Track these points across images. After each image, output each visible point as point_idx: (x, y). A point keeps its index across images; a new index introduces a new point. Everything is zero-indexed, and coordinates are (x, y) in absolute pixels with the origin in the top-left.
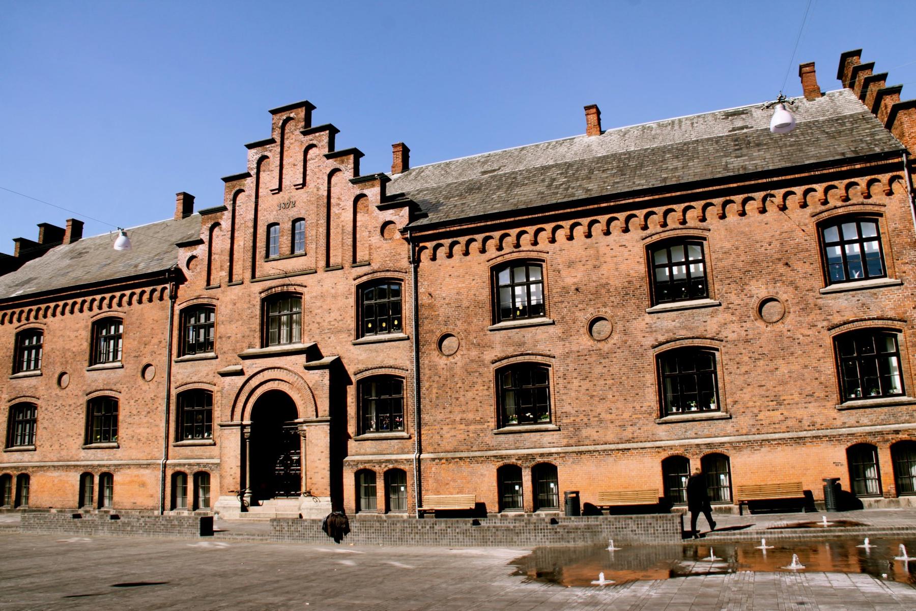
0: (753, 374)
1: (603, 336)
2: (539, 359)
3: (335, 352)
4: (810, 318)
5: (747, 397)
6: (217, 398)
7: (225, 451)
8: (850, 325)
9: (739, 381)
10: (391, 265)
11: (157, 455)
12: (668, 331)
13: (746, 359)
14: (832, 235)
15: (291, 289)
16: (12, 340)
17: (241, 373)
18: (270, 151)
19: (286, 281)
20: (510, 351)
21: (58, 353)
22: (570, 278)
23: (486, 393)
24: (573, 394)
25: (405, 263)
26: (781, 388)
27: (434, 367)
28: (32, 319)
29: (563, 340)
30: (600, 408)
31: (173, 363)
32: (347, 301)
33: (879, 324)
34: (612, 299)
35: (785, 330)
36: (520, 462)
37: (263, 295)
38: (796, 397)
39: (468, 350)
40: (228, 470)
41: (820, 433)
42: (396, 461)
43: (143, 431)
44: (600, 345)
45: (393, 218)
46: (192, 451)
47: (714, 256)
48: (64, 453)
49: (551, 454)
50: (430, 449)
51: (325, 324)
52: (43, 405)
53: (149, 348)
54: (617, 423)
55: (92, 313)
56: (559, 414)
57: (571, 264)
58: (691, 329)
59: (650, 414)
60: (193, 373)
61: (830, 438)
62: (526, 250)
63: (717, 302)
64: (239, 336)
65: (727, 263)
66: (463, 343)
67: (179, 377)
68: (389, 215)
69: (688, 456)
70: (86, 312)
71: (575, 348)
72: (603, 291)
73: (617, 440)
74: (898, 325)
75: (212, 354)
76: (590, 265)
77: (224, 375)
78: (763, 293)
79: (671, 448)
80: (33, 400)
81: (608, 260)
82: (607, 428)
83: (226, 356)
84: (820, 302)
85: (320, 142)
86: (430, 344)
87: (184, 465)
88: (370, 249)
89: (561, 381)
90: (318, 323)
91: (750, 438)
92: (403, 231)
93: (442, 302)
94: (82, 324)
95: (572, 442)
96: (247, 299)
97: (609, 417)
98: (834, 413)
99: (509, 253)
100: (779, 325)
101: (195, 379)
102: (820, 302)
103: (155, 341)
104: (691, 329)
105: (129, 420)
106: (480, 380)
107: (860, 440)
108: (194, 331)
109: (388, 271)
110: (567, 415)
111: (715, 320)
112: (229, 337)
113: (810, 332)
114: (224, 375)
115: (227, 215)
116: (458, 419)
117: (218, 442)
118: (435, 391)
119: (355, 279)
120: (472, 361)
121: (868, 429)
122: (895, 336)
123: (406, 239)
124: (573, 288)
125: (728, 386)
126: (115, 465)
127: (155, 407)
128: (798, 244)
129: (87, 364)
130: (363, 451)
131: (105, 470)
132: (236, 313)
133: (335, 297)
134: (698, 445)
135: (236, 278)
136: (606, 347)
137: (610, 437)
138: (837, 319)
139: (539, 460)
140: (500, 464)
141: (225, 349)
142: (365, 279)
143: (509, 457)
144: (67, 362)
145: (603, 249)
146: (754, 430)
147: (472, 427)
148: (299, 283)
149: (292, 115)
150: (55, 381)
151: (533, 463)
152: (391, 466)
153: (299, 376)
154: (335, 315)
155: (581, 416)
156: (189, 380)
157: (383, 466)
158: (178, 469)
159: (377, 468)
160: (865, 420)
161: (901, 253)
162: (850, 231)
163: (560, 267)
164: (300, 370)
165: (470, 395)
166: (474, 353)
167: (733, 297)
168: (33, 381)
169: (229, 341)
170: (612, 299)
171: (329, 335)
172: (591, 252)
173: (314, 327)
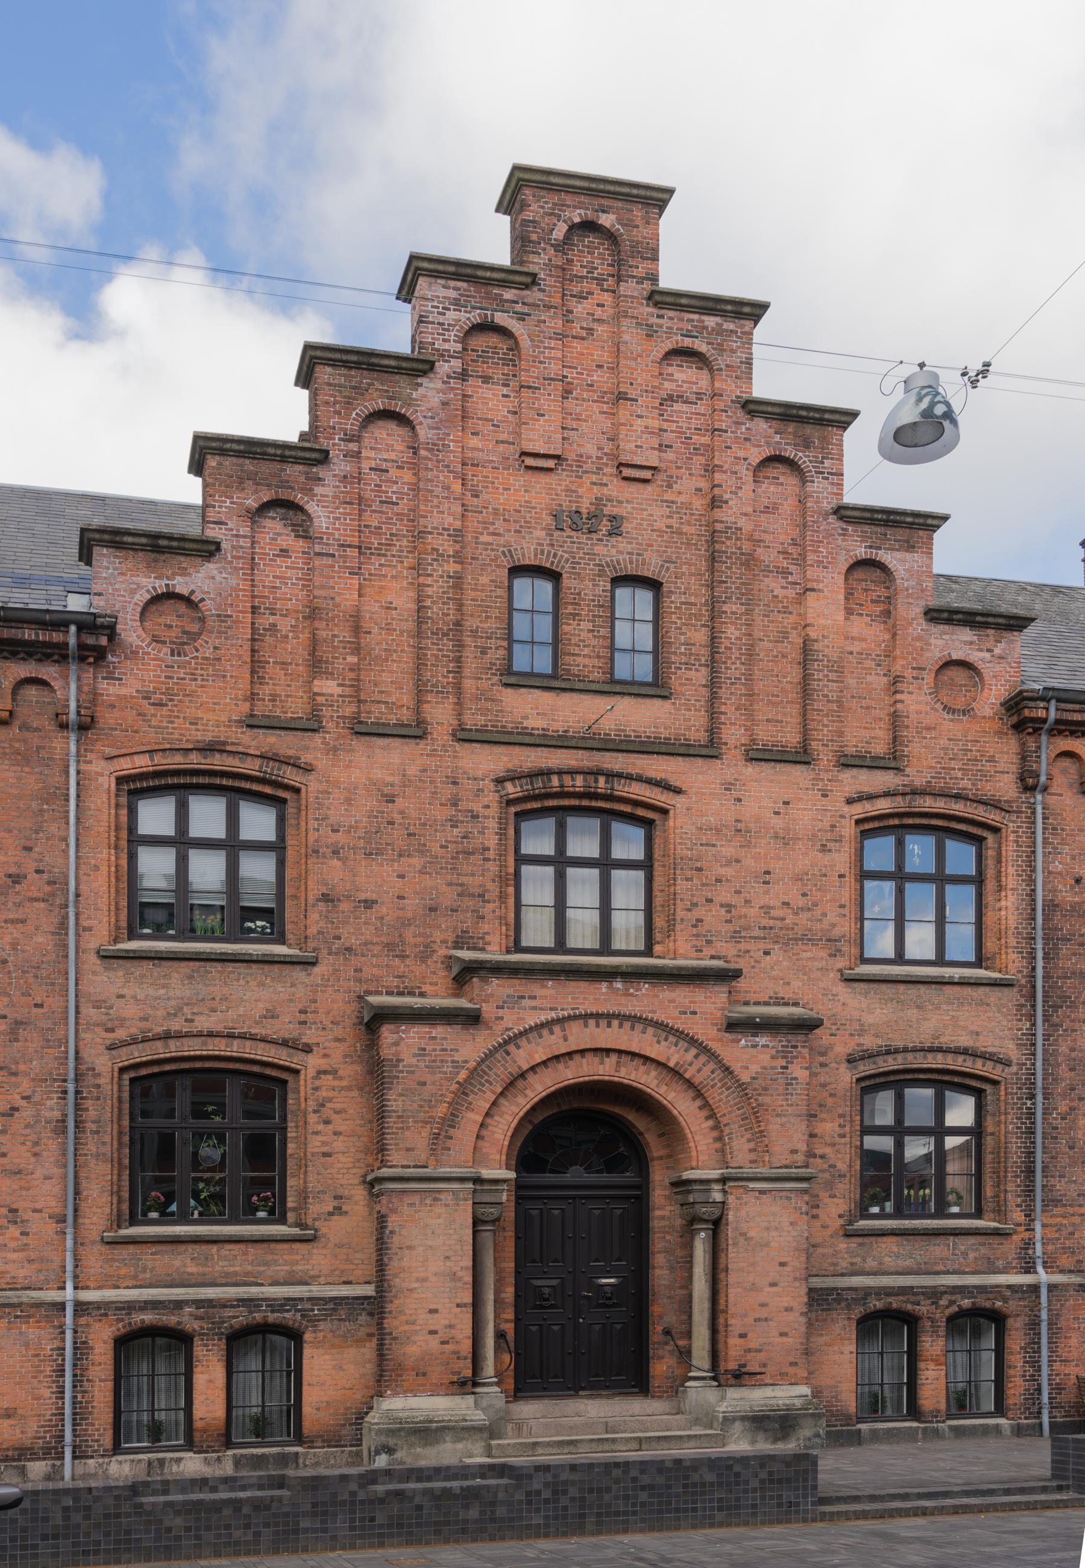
10: (966, 783)
14: (156, 816)
18: (521, 317)
25: (1006, 787)
32: (826, 859)
37: (512, 789)
40: (423, 1317)
42: (982, 1289)
45: (975, 656)
51: (753, 912)
64: (413, 904)
67: (130, 1010)
83: (355, 961)
87: (179, 1305)
90: (728, 907)
96: (448, 791)
101: (204, 1023)
109: (957, 797)
112: (369, 904)
119: (850, 801)
130: (871, 1264)
133: (785, 840)
149: (607, 220)
152: (966, 1303)
156: (176, 1025)
157: (943, 1302)
159: (924, 1308)
162: (207, 816)
169: (372, 915)
171: (762, 945)
173: (713, 917)
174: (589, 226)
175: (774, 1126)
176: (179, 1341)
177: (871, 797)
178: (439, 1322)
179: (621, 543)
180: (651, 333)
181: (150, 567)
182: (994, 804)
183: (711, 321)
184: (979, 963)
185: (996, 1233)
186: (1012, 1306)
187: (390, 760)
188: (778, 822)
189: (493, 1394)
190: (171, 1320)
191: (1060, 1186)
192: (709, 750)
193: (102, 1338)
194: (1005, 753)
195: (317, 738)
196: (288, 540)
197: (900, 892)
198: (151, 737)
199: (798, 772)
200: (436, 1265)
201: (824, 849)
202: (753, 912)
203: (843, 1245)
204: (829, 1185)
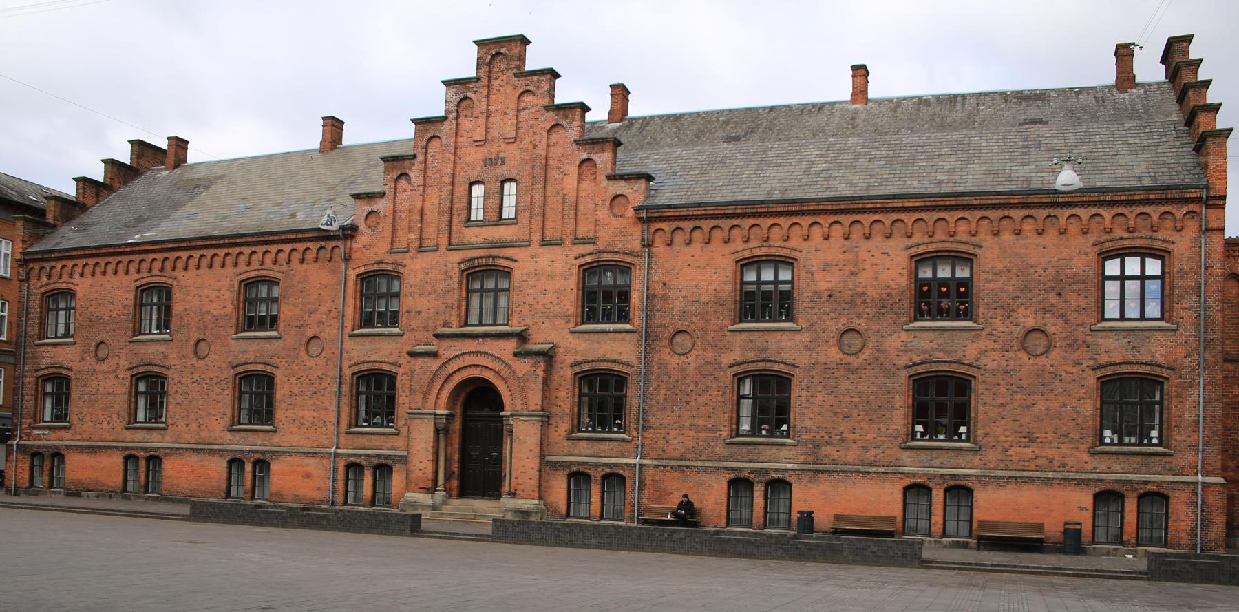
0: (1008, 408)
1: (854, 349)
2: (782, 368)
3: (549, 339)
4: (1076, 355)
5: (999, 430)
6: (402, 381)
7: (417, 442)
8: (1117, 367)
9: (993, 413)
11: (326, 442)
12: (924, 352)
13: (1003, 390)
15: (502, 262)
16: (131, 296)
17: (434, 355)
18: (475, 92)
19: (496, 252)
20: (751, 355)
21: (193, 315)
22: (824, 283)
23: (719, 398)
24: (816, 409)
25: (636, 246)
26: (1035, 425)
27: (663, 366)
28: (156, 271)
29: (810, 350)
30: (843, 426)
31: (346, 337)
32: (566, 283)
33: (1147, 369)
34: (868, 310)
35: (1048, 365)
36: (752, 476)
37: (463, 266)
38: (1050, 436)
39: (704, 350)
41: (1071, 475)
42: (615, 465)
43: (308, 415)
44: (849, 359)
45: (626, 192)
46: (370, 441)
47: (983, 276)
48: (204, 434)
49: (787, 470)
50: (653, 454)
52: (175, 376)
53: (316, 317)
54: (860, 444)
55: (237, 270)
56: (798, 428)
57: (826, 267)
58: (949, 353)
59: (896, 438)
60: (379, 350)
61: (1079, 482)
62: (777, 247)
63: (981, 327)
65: (996, 285)
66: (699, 342)
67: (355, 354)
68: (620, 187)
69: (931, 485)
70: (230, 270)
71: (822, 359)
72: (859, 301)
73: (857, 462)
74: (1165, 373)
75: (396, 330)
76: (846, 272)
77: (413, 354)
78: (1030, 322)
79: (914, 475)
80: (162, 371)
81: (868, 267)
82: (848, 448)
84: (1089, 339)
85: (538, 88)
86: (661, 340)
87: (361, 455)
88: (596, 225)
89: (804, 393)
91: (999, 473)
92: (637, 209)
93: (678, 294)
94: (225, 282)
95: (810, 459)
97: (852, 436)
98: (1086, 457)
99: (756, 248)
100: (1043, 358)
101: (374, 358)
102: (1089, 339)
103: (323, 309)
104: (949, 353)
105: (289, 401)
106: (714, 385)
107: (1108, 487)
108: (377, 297)
110: (807, 430)
111: (975, 345)
112: (419, 312)
113: (1074, 370)
114: (413, 354)
115: (417, 165)
116: (687, 424)
117: (404, 430)
118: (663, 392)
120: (708, 363)
121: (1118, 476)
122: (1162, 383)
123: (640, 219)
124: (826, 294)
125: (981, 417)
126: (271, 452)
127: (322, 387)
128: (1075, 274)
129: (232, 331)
130: (576, 452)
131: (260, 456)
132: (427, 284)
133: (551, 276)
134: (942, 475)
135: (426, 243)
136: (855, 362)
137: (851, 457)
138: (1104, 359)
139: (774, 475)
140: (731, 476)
141: (414, 326)
142: (588, 259)
143: (740, 469)
144: (206, 327)
145: (863, 255)
146: (1002, 466)
147: (702, 435)
148: (508, 255)
149: (503, 50)
150: (190, 349)
151: (767, 478)
152: (608, 470)
153: (507, 365)
154: (551, 297)
155: (823, 433)
156: (366, 359)
158: (352, 459)
159: (591, 472)
160: (1117, 467)
161: (1181, 297)
163: (814, 269)
164: (508, 357)
165: (702, 399)
166: (710, 354)
167: (997, 323)
168: (161, 348)
169: (419, 317)
170: (868, 310)
172: (849, 256)
173: (525, 309)
174: (498, 54)
175: (530, 394)
176: (135, 458)
177: (583, 256)
178: (422, 466)
179: (504, 167)
180: (515, 87)
181: (368, 204)
182: (630, 254)
183: (535, 78)
184: (1162, 319)
185: (624, 440)
186: (626, 473)
187: (427, 260)
188: (549, 269)
189: (440, 495)
190: (358, 461)
191: (652, 420)
192: (526, 244)
193: (341, 465)
194: (636, 232)
195: (407, 255)
196: (407, 186)
197: (481, 296)
198: (365, 261)
199: (557, 248)
200: (422, 445)
201: (566, 279)
202: (539, 306)
203: (566, 443)
204: (562, 418)
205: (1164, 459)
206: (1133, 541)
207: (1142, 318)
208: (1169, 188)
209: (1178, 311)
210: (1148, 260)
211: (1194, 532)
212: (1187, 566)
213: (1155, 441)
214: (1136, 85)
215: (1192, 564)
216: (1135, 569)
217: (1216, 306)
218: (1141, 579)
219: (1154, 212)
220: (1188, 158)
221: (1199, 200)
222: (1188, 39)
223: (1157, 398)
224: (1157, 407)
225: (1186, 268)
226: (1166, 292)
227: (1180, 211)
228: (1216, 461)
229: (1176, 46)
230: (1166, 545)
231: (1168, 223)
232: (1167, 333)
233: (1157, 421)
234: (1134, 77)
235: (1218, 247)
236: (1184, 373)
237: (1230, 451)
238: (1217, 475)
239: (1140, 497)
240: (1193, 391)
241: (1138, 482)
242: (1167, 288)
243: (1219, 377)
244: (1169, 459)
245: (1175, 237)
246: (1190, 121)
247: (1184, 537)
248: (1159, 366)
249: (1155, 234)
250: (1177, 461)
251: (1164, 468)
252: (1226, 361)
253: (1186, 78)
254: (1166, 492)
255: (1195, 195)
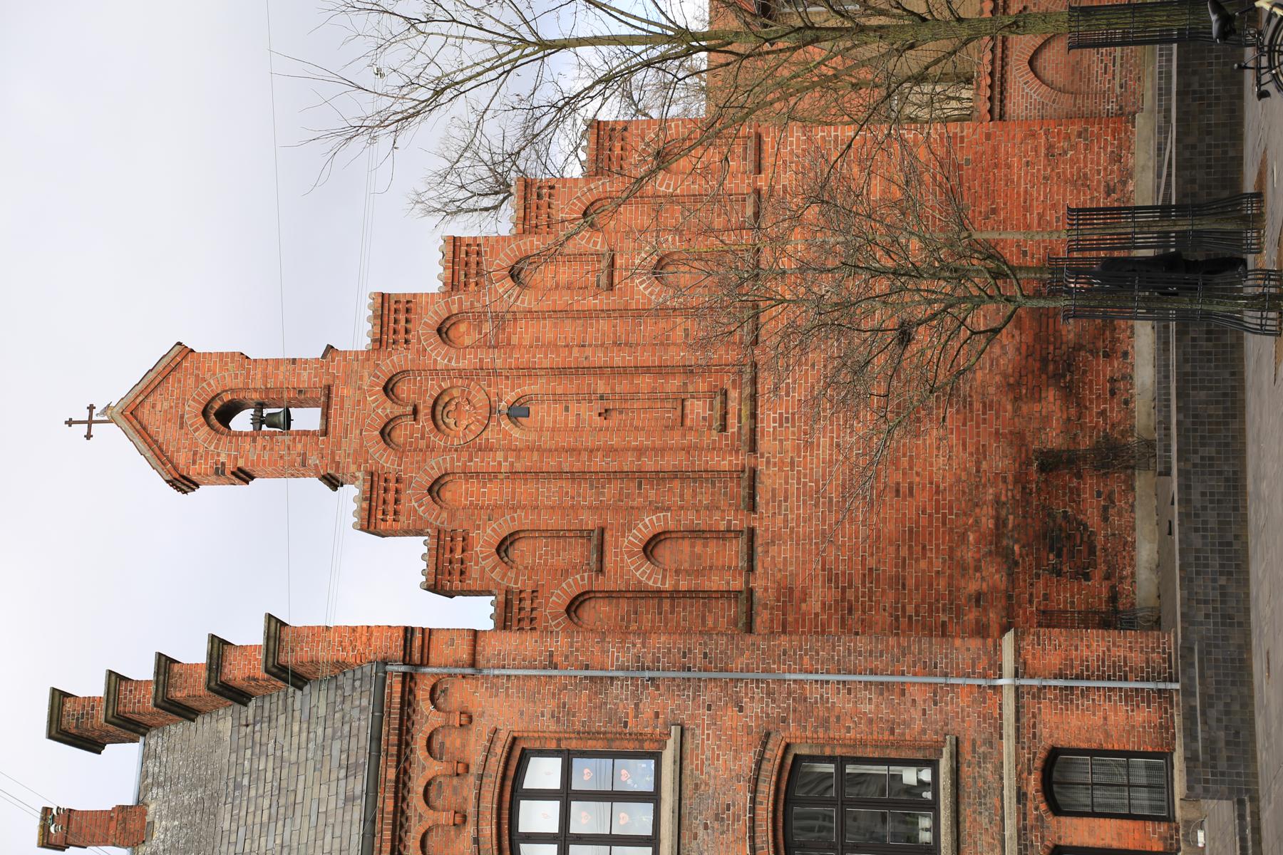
33: (766, 789)
184: (656, 756)
205: (966, 755)
206: (1163, 828)
207: (653, 797)
208: (376, 738)
209: (643, 723)
210: (523, 828)
211: (1129, 696)
212: (1213, 713)
213: (926, 775)
214: (141, 805)
215: (1207, 703)
216: (1232, 828)
217: (636, 647)
218: (1256, 815)
219: (424, 768)
220: (317, 700)
221: (408, 680)
222: (59, 698)
223: (830, 768)
224: (850, 769)
225: (551, 705)
226: (599, 746)
227: (427, 717)
228: (966, 649)
229: (69, 723)
230: (1167, 756)
231: (452, 741)
232: (688, 746)
233: (881, 770)
234: (122, 809)
235: (511, 642)
236: (774, 710)
237: (943, 617)
238: (997, 648)
239: (1056, 809)
240: (814, 694)
241: (1023, 815)
242: (591, 745)
243: (784, 641)
244: (966, 747)
245: (482, 728)
246: (239, 696)
247: (1144, 715)
248: (759, 764)
249: (474, 769)
250: (971, 729)
251: (985, 756)
252: (749, 628)
253: (145, 703)
254: (1042, 754)
255: (398, 688)
